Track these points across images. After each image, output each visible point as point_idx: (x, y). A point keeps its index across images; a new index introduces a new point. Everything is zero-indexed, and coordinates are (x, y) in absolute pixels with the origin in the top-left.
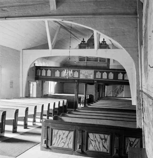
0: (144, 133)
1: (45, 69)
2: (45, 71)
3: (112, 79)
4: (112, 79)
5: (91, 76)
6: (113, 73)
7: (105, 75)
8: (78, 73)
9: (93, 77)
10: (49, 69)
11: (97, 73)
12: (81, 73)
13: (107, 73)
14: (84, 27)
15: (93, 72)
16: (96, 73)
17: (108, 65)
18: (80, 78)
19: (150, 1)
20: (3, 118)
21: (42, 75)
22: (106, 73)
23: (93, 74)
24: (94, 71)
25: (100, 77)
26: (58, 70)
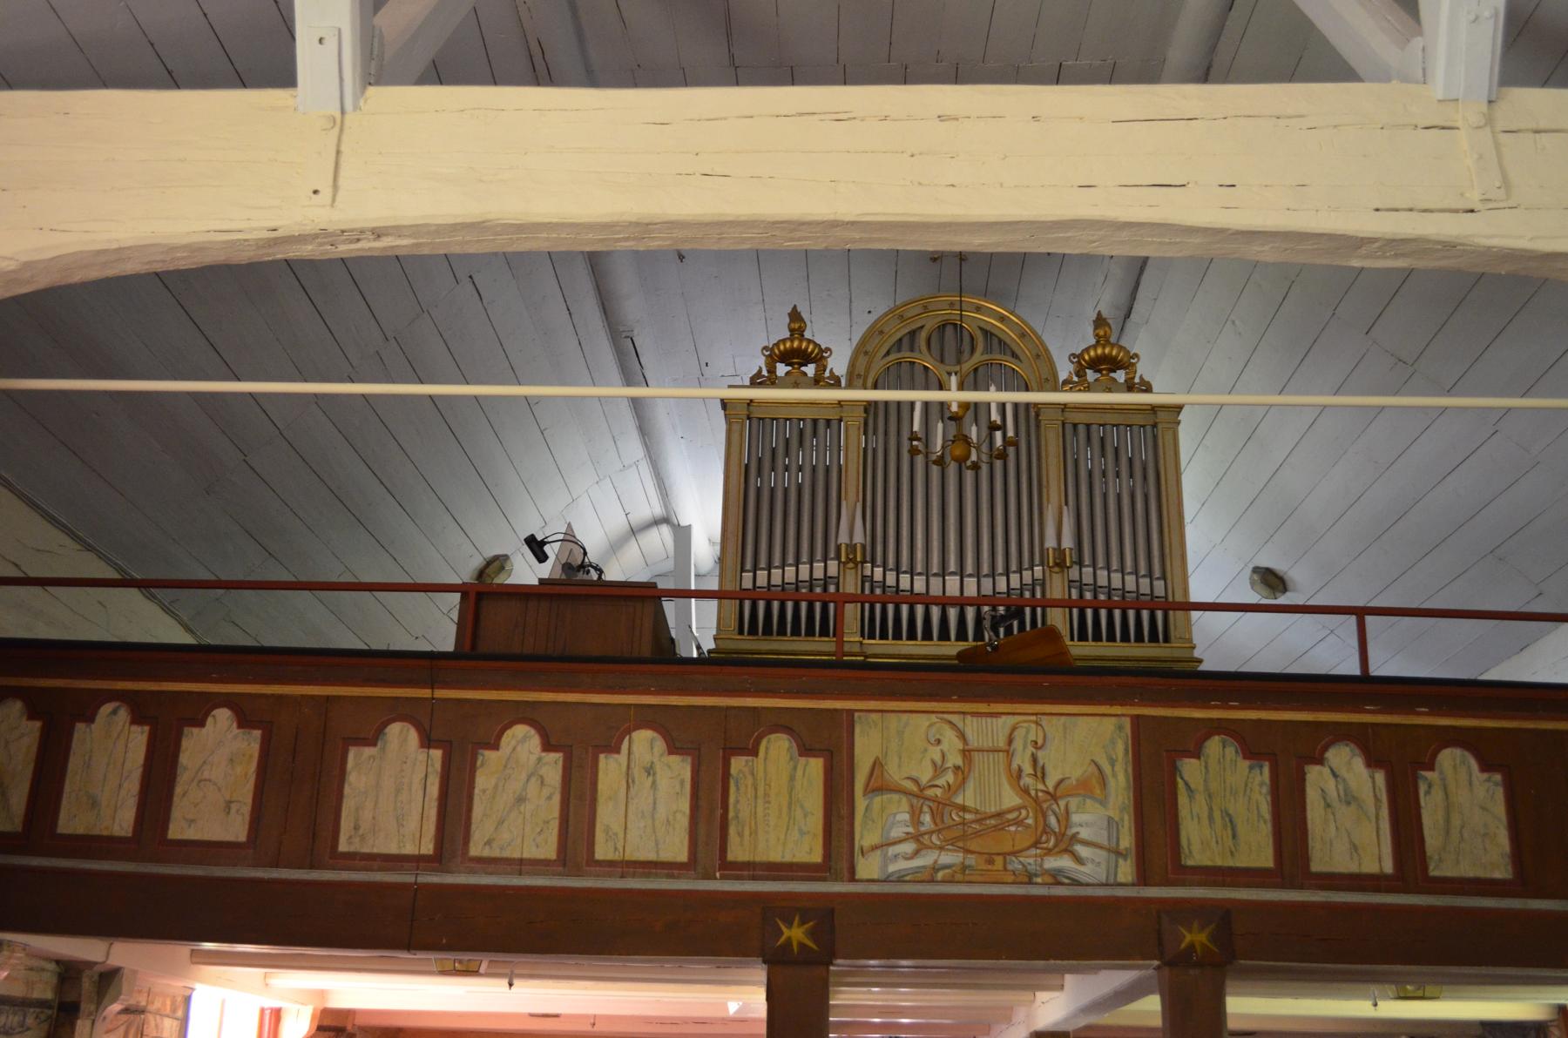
0: (302, 239)
1: (141, 708)
2: (139, 737)
3: (1502, 871)
4: (1502, 871)
5: (1088, 821)
6: (1486, 767)
7: (1349, 799)
8: (816, 766)
9: (1127, 841)
10: (209, 703)
11: (1190, 768)
12: (877, 765)
13: (1372, 762)
14: (1134, 960)
15: (1121, 749)
16: (1174, 771)
17: (42, 1004)
18: (868, 868)
19: (1235, 3)
20: (830, 836)
21: (72, 821)
22: (1359, 764)
23: (1120, 782)
24: (1136, 720)
25: (1258, 851)
26: (780, 723)
